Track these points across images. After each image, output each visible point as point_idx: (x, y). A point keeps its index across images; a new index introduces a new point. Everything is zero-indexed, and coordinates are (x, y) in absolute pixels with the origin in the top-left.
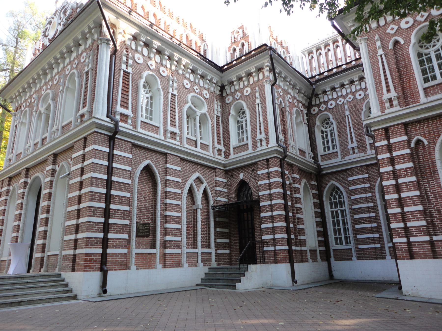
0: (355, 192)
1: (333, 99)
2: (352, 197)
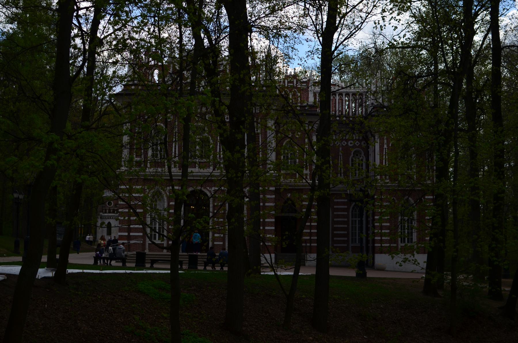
2: (335, 213)
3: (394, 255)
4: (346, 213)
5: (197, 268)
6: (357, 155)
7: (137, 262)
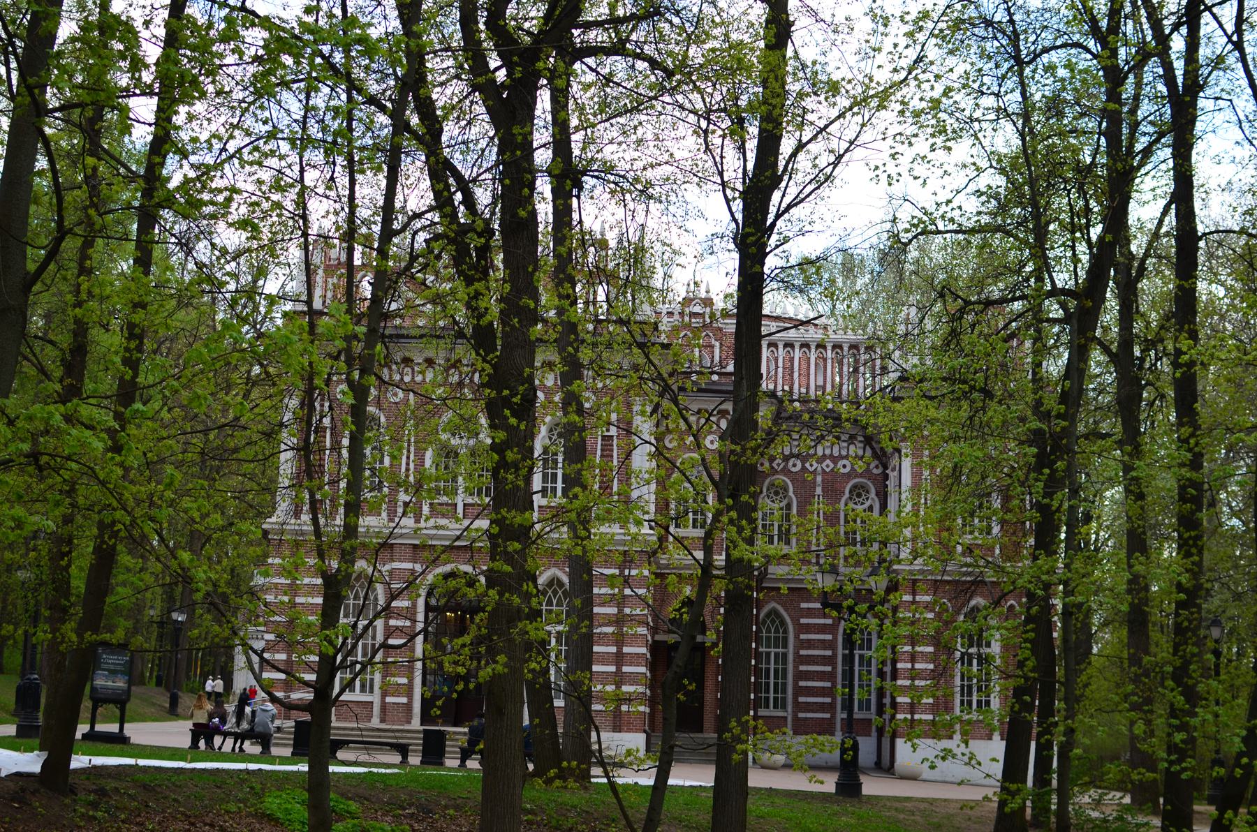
0: (809, 628)
1: (832, 457)
2: (803, 637)
3: (916, 741)
4: (829, 637)
5: (442, 764)
6: (859, 495)
7: (295, 746)
